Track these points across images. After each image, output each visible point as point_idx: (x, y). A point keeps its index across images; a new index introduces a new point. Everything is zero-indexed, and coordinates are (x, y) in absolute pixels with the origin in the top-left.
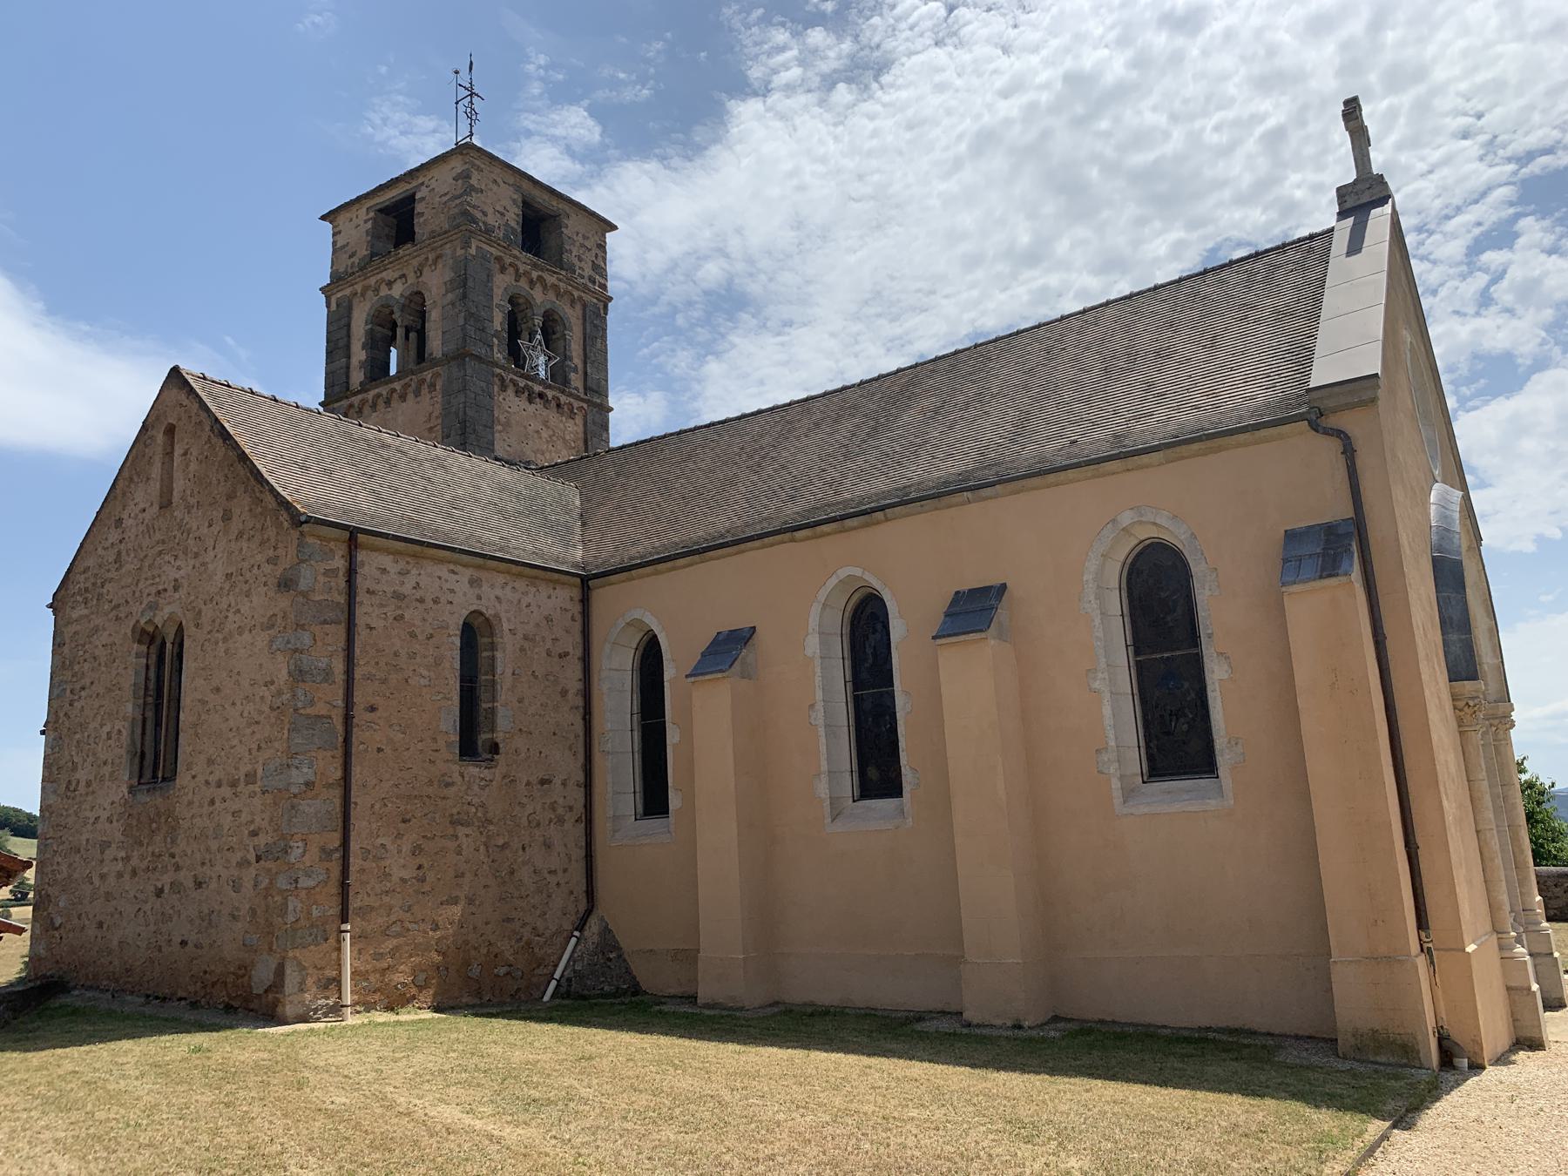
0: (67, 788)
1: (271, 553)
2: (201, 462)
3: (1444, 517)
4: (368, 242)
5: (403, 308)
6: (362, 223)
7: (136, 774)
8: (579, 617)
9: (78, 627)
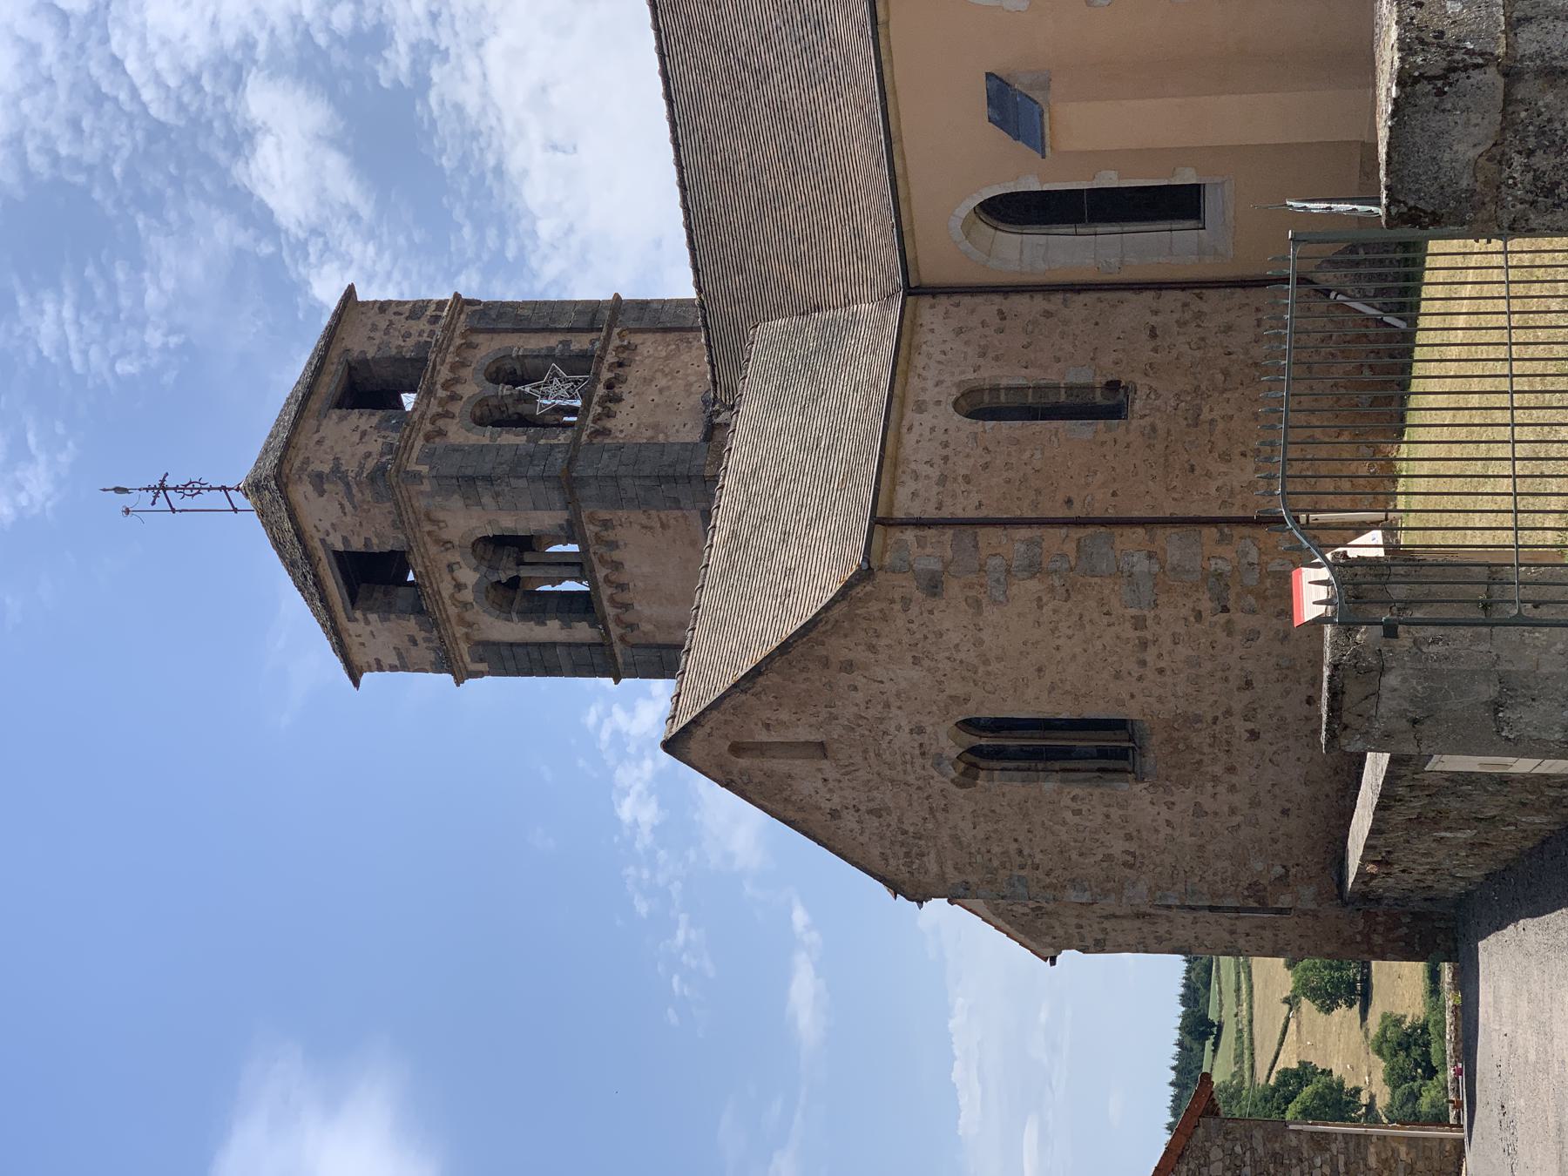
1: (897, 607)
2: (780, 705)
6: (369, 628)
7: (1121, 776)
8: (956, 299)
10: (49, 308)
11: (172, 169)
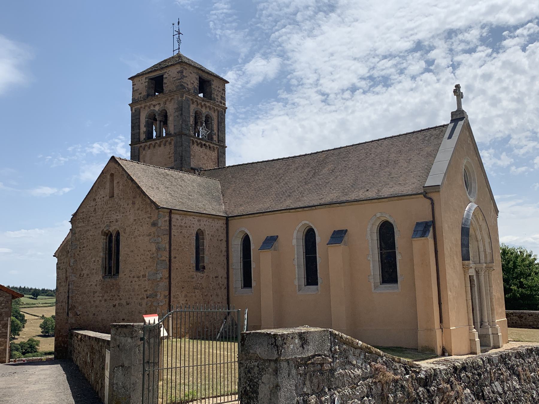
0: (80, 276)
1: (149, 215)
3: (468, 215)
4: (146, 90)
5: (159, 115)
6: (144, 82)
8: (225, 229)
9: (81, 229)
10: (226, 6)
11: (259, 39)
